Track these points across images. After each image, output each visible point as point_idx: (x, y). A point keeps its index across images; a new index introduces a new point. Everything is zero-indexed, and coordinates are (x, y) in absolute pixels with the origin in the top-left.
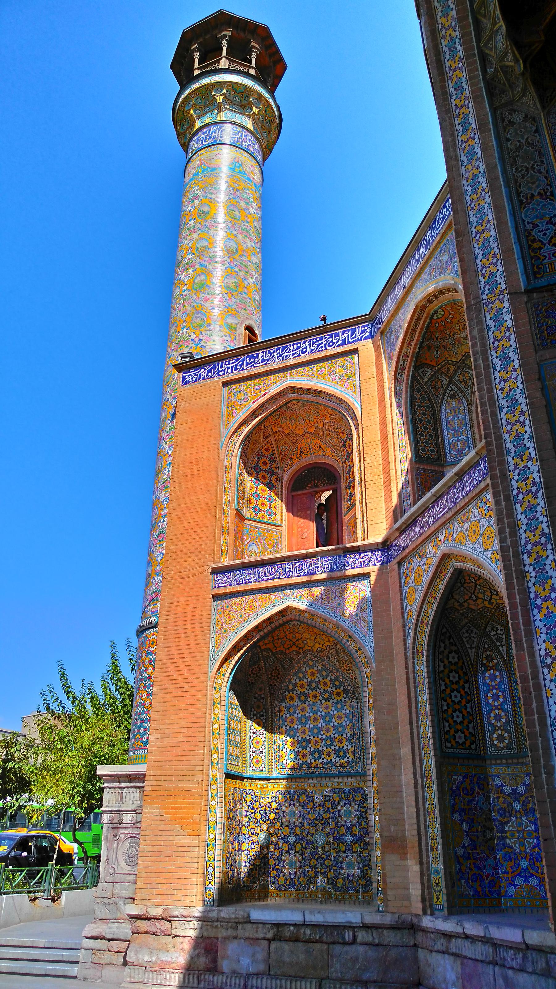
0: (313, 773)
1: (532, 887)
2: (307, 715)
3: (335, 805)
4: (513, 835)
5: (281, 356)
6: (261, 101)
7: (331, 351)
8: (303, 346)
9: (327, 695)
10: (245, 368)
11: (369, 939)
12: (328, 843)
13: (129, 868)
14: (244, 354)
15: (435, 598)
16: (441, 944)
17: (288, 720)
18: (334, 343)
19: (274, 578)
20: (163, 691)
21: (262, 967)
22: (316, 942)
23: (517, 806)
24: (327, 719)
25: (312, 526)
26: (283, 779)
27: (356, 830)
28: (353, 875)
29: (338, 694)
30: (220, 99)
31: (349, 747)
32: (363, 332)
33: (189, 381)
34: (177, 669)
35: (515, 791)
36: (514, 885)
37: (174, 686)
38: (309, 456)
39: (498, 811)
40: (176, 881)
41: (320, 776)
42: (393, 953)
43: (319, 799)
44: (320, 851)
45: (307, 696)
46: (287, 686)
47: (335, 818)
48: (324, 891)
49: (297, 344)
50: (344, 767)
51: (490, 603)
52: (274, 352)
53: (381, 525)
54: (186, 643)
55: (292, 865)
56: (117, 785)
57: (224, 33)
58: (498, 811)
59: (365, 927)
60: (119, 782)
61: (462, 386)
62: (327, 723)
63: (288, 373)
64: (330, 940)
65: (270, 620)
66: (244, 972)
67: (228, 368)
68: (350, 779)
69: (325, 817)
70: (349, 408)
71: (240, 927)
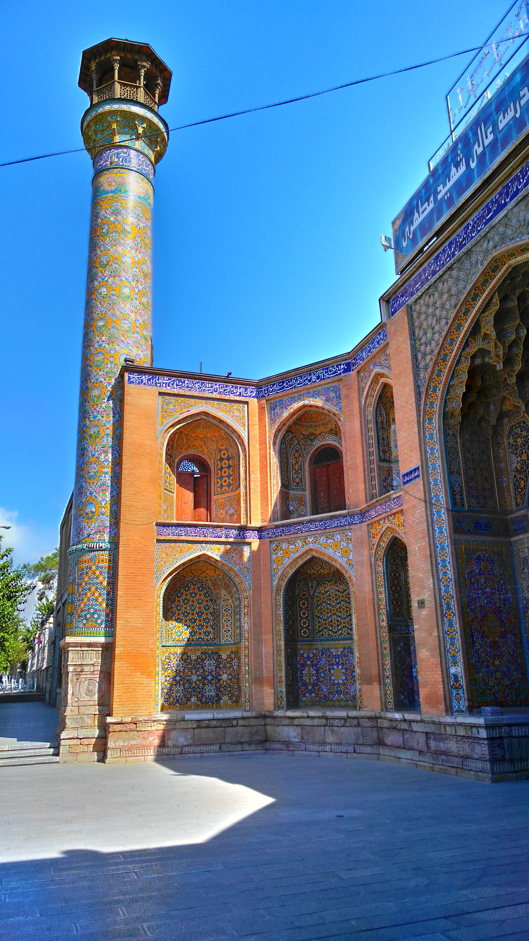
0: (190, 643)
1: (312, 697)
2: (188, 611)
3: (203, 660)
4: (306, 675)
5: (200, 388)
6: (163, 142)
7: (232, 397)
8: (215, 387)
9: (200, 601)
10: (175, 387)
11: (244, 723)
12: (198, 680)
13: (89, 697)
14: (174, 377)
15: (295, 566)
16: (287, 722)
17: (177, 613)
18: (234, 393)
19: (196, 536)
20: (124, 595)
21: (190, 742)
22: (219, 727)
23: (309, 663)
24: (200, 614)
25: (192, 495)
26: (181, 646)
27: (214, 673)
28: (211, 696)
29: (207, 601)
30: (140, 130)
31: (212, 630)
32: (252, 392)
33: (133, 382)
34: (134, 582)
35: (308, 656)
36: (305, 697)
37: (132, 592)
38: (192, 450)
39: (301, 665)
40: (140, 702)
41: (195, 645)
42: (255, 729)
43: (194, 658)
44: (194, 684)
45: (189, 600)
46: (177, 594)
47: (203, 667)
48: (195, 704)
49: (211, 384)
50: (208, 641)
51: (318, 572)
52: (196, 383)
53: (258, 516)
54: (140, 567)
55: (178, 692)
56: (79, 649)
57: (144, 64)
58: (301, 665)
59: (243, 718)
60: (81, 647)
61: (303, 447)
62: (200, 617)
63: (203, 401)
64: (226, 726)
65: (191, 560)
66: (181, 745)
67: (163, 383)
68: (211, 647)
69: (197, 666)
70: (239, 437)
71: (178, 723)
